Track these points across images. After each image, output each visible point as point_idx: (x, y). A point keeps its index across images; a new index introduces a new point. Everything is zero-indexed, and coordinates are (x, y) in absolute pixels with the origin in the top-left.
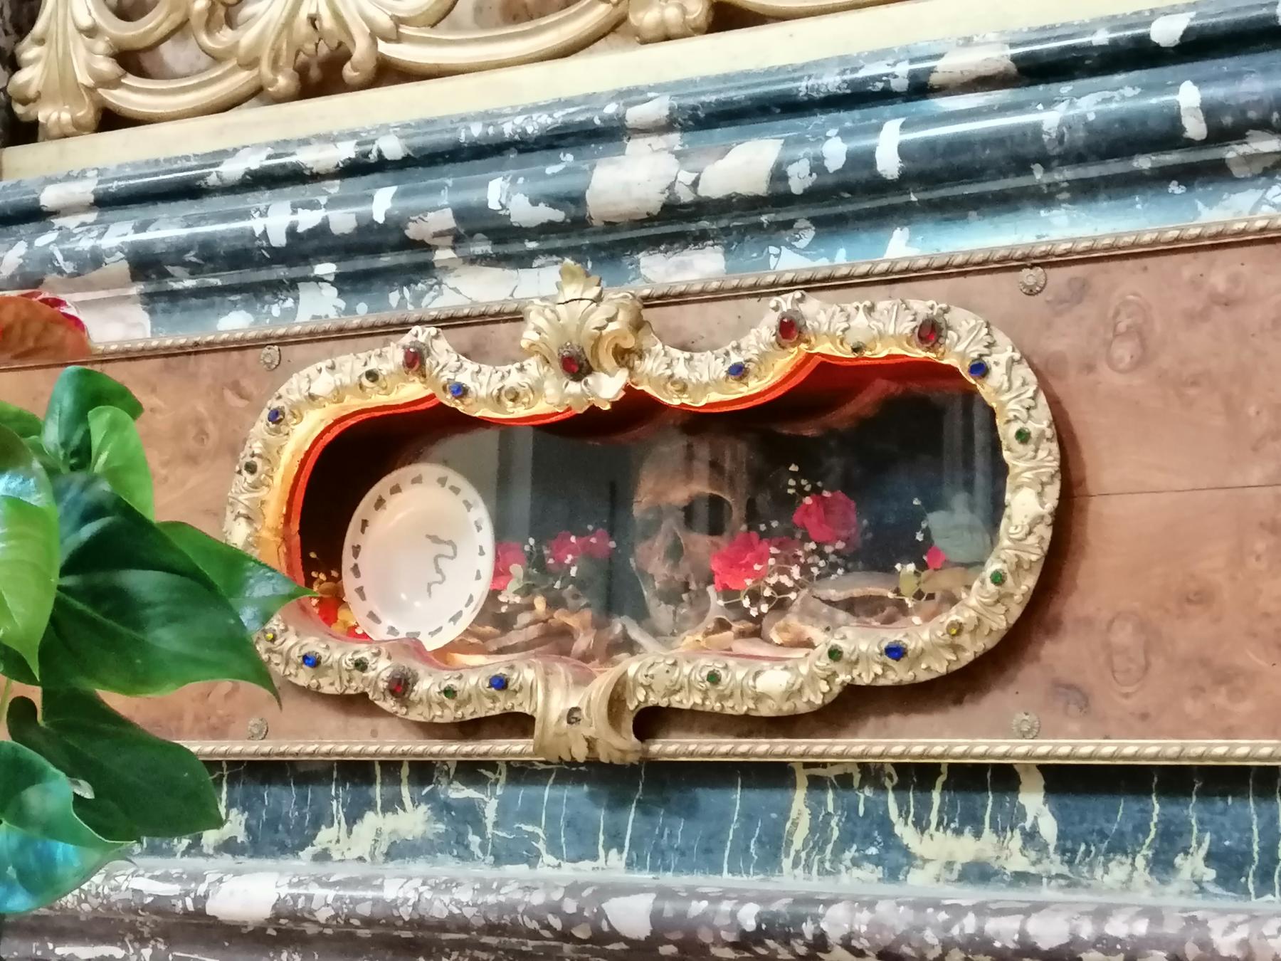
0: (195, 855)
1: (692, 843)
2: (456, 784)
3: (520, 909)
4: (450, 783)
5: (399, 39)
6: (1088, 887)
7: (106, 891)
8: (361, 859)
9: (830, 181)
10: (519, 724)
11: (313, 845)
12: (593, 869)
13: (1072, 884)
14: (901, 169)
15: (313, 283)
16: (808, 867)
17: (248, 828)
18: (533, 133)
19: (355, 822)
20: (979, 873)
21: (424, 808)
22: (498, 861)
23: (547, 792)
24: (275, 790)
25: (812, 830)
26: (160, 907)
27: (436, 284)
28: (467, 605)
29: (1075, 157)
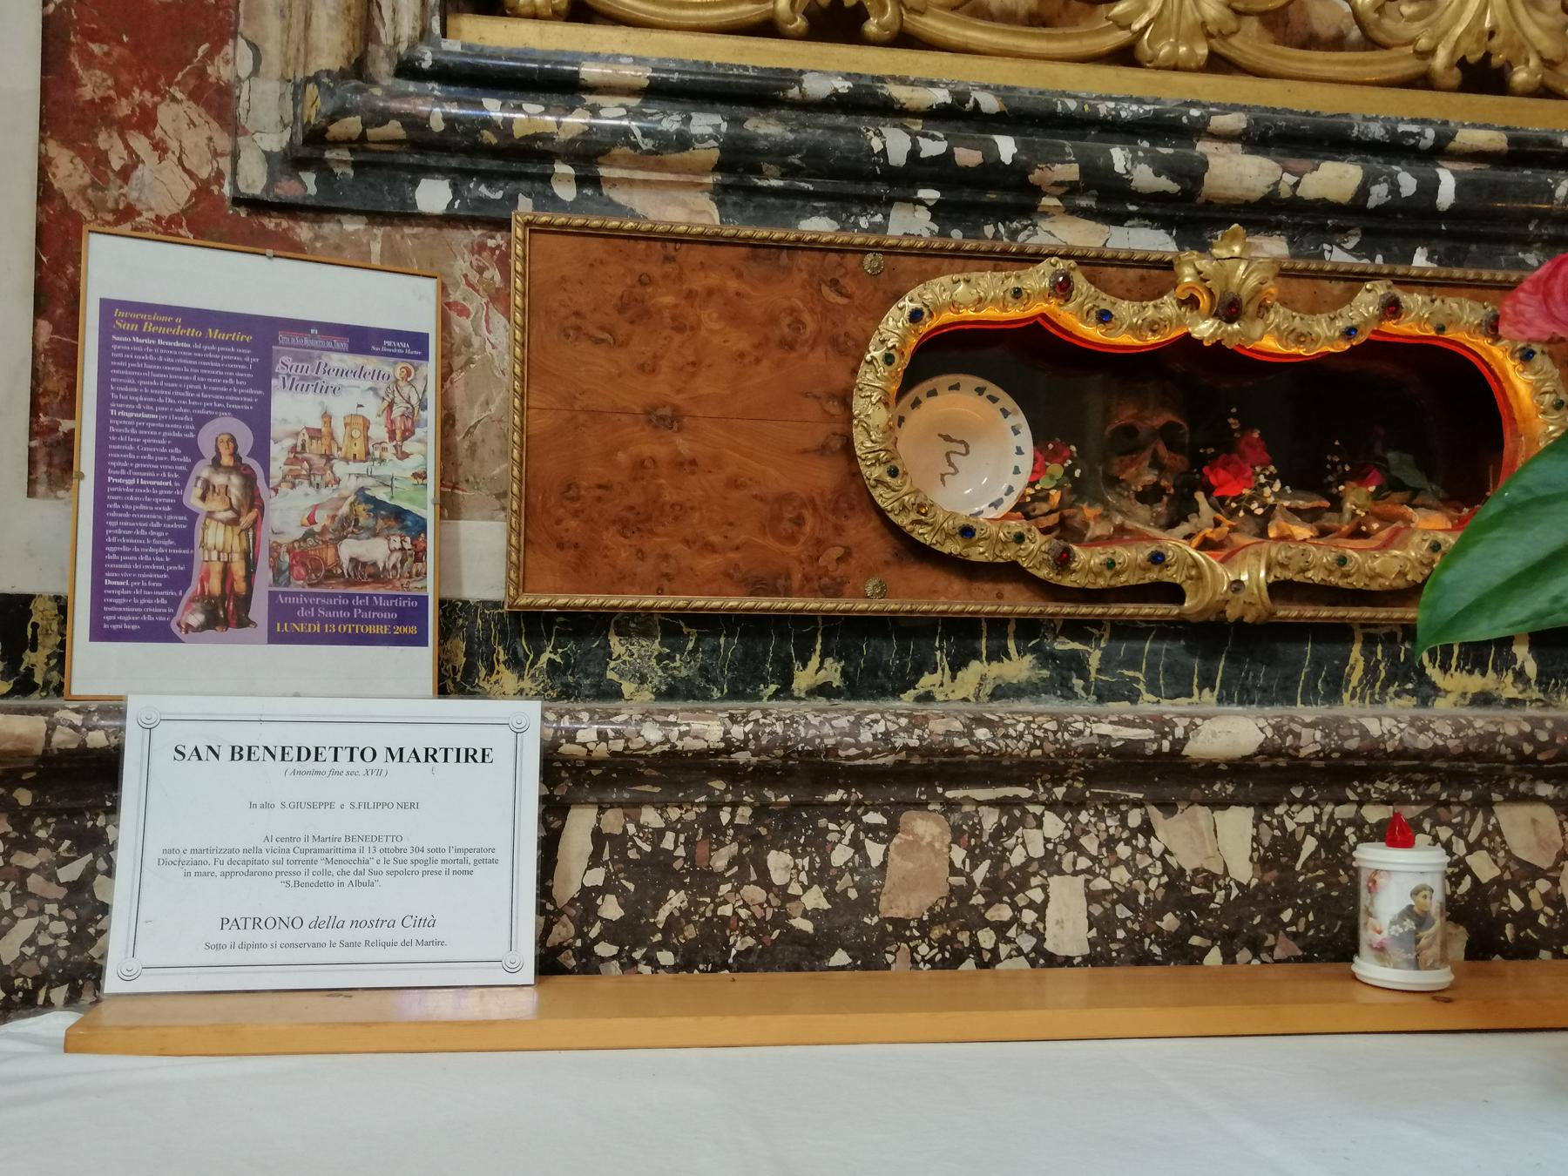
0: (785, 699)
3: (1499, 739)
6: (1556, 707)
7: (1067, 737)
8: (965, 700)
10: (1174, 593)
13: (1546, 705)
16: (1362, 699)
17: (844, 673)
20: (1484, 699)
21: (1029, 657)
22: (1101, 699)
25: (1366, 672)
26: (1130, 751)
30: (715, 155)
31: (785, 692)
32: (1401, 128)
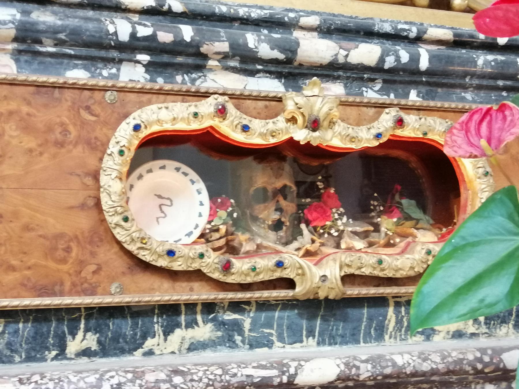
0: (62, 359)
1: (346, 332)
2: (228, 313)
3: (465, 362)
4: (225, 312)
6: (494, 336)
8: (173, 353)
9: (400, 66)
10: (290, 284)
11: (142, 348)
12: (301, 347)
13: (490, 335)
14: (428, 67)
15: (133, 63)
16: (395, 338)
17: (99, 342)
18: (254, 17)
19: (169, 335)
21: (210, 325)
22: (252, 347)
23: (277, 314)
24: (117, 321)
25: (397, 323)
27: (203, 76)
28: (195, 229)
29: (483, 76)
30: (13, 33)
31: (62, 354)
32: (400, 26)
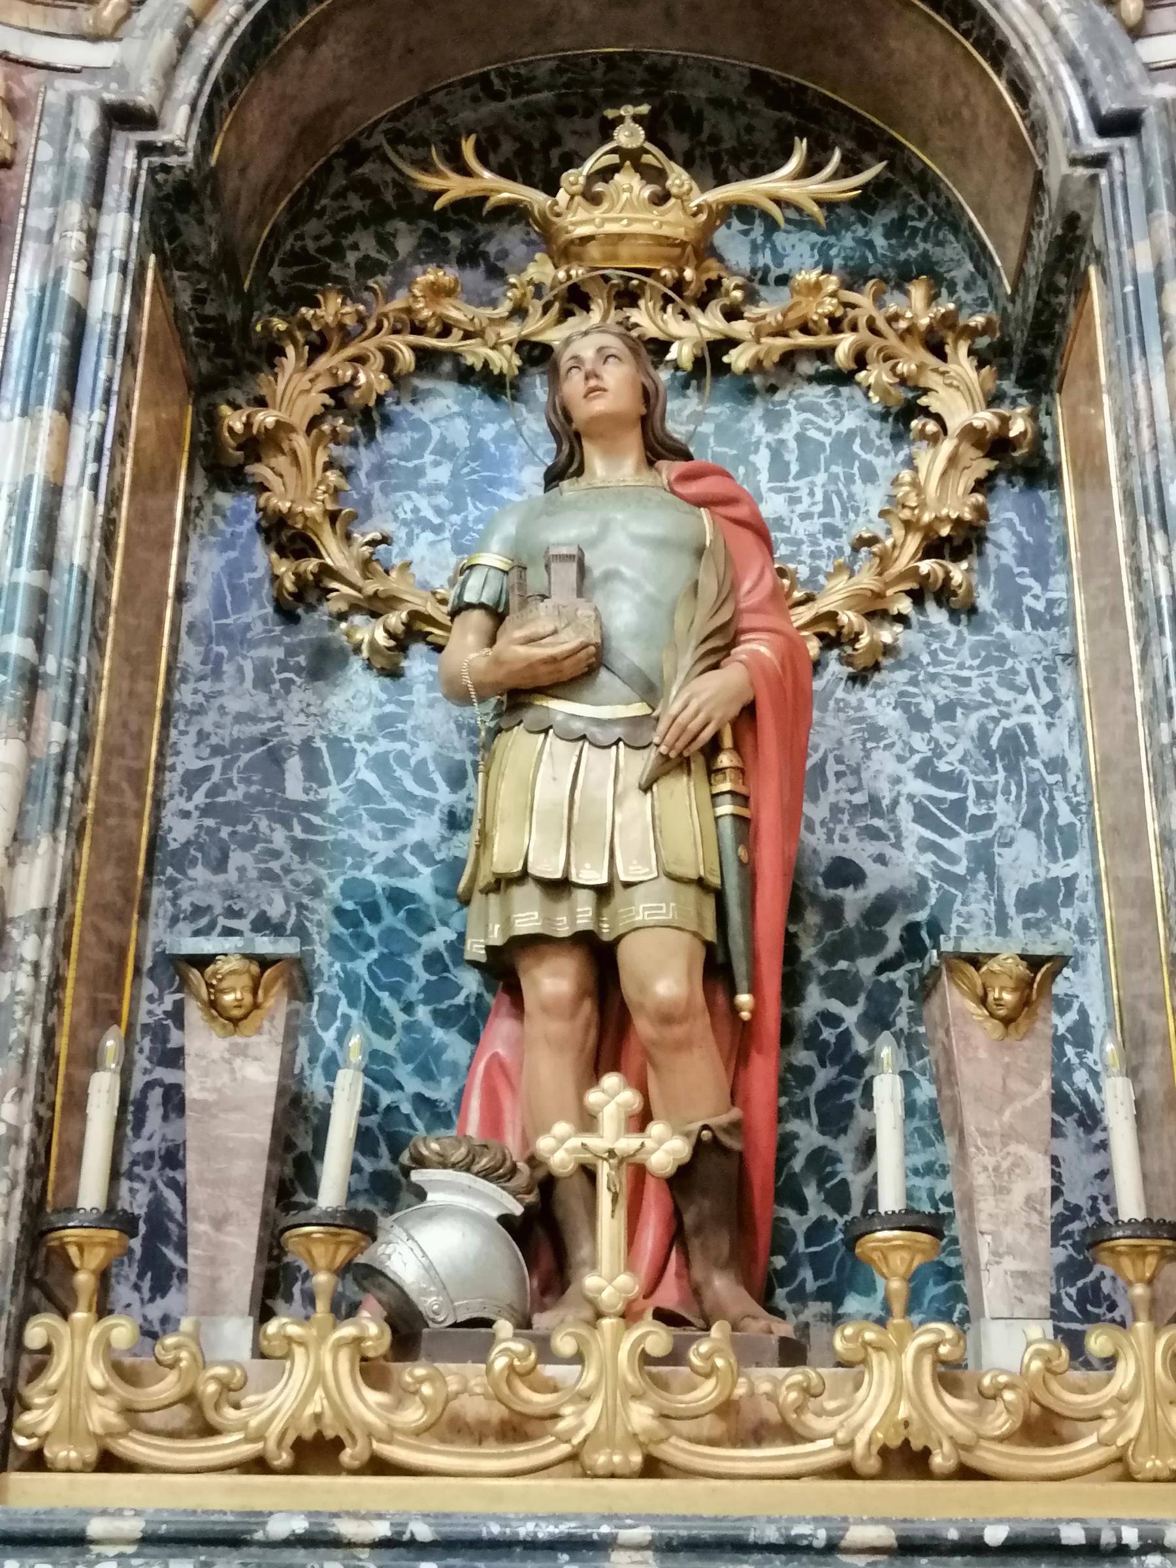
5: (389, 1442)
32: (797, 1530)
